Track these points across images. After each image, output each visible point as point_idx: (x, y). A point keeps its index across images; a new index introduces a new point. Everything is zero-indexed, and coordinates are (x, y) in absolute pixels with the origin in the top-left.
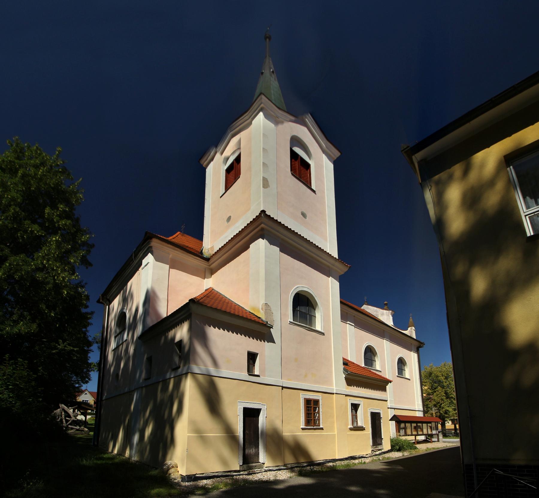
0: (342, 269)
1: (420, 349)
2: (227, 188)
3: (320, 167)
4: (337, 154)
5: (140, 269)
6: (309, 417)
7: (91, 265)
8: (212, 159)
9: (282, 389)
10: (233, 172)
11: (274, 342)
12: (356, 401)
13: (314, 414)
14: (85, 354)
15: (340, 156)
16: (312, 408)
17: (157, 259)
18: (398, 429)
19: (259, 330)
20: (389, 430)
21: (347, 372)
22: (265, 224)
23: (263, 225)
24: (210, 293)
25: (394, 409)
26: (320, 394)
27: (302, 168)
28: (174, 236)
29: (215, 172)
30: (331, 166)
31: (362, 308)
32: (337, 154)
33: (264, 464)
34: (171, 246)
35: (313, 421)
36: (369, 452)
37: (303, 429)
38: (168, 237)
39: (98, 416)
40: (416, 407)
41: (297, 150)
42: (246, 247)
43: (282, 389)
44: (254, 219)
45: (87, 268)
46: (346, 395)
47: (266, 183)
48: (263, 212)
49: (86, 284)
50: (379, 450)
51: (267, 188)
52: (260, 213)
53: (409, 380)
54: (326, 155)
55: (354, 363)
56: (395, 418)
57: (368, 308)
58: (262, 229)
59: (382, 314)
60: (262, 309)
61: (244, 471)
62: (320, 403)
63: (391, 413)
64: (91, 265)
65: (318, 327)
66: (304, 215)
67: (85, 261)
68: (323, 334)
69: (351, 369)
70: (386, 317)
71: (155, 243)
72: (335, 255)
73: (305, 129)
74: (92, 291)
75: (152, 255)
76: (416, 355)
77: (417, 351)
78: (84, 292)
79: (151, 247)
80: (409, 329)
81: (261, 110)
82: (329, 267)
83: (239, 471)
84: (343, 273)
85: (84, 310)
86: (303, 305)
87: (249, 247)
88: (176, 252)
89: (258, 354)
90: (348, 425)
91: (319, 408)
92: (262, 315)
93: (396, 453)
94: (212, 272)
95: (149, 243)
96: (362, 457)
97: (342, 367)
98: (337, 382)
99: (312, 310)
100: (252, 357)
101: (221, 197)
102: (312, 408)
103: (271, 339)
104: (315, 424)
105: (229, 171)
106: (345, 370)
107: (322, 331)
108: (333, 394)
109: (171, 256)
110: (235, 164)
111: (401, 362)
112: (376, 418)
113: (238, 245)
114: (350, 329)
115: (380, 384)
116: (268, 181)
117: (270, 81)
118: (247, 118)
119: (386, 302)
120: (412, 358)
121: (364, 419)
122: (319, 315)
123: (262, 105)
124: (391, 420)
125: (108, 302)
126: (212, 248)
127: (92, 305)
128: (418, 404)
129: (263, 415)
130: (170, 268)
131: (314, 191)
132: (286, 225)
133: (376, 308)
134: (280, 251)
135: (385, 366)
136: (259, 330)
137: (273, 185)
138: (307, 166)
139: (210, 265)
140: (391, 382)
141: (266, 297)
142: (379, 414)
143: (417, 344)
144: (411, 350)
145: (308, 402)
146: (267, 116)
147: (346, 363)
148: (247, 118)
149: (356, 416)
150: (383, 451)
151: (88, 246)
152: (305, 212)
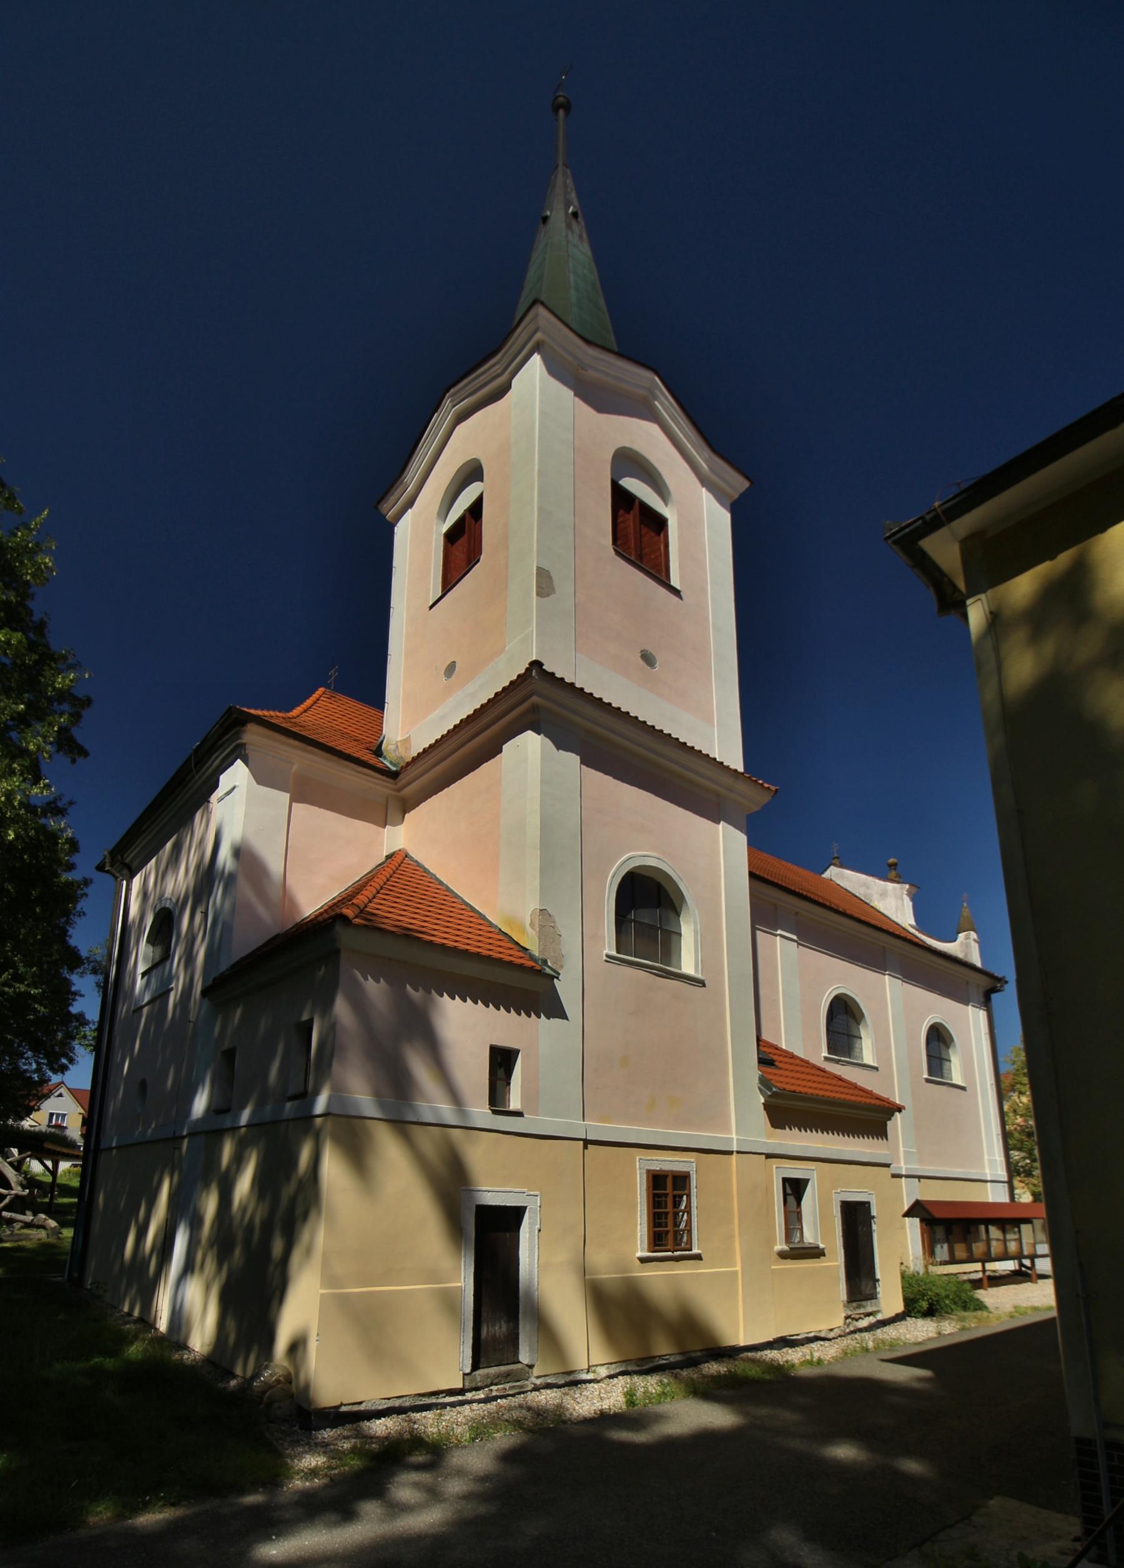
0: (755, 798)
1: (994, 996)
2: (448, 584)
3: (691, 523)
4: (739, 484)
5: (214, 798)
6: (660, 1225)
7: (84, 753)
8: (410, 503)
9: (585, 1147)
10: (463, 543)
11: (563, 1016)
12: (796, 1171)
13: (676, 1214)
14: (63, 994)
15: (748, 489)
16: (667, 1195)
17: (262, 777)
18: (929, 1249)
19: (525, 986)
20: (900, 1248)
21: (770, 1089)
22: (540, 695)
23: (535, 699)
24: (398, 861)
25: (920, 1177)
26: (692, 1157)
27: (645, 530)
28: (309, 702)
29: (416, 540)
30: (724, 518)
31: (826, 875)
32: (739, 484)
33: (531, 1367)
34: (296, 743)
35: (670, 1236)
36: (838, 1321)
37: (643, 1260)
38: (290, 710)
39: (89, 1174)
40: (987, 1171)
41: (633, 485)
42: (493, 750)
43: (585, 1147)
44: (512, 683)
45: (74, 761)
46: (769, 1156)
47: (545, 584)
48: (536, 664)
49: (71, 803)
50: (868, 1315)
51: (548, 595)
52: (527, 669)
53: (963, 1088)
54: (709, 490)
55: (793, 1056)
56: (917, 1209)
57: (842, 877)
58: (535, 708)
59: (883, 894)
60: (532, 925)
61: (477, 1389)
62: (693, 1183)
63: (908, 1193)
64: (84, 753)
65: (688, 966)
66: (648, 659)
67: (67, 744)
68: (702, 983)
69: (784, 1081)
70: (893, 902)
71: (252, 735)
72: (736, 762)
73: (654, 429)
74: (88, 831)
75: (246, 763)
76: (982, 1015)
77: (986, 1002)
78: (62, 830)
79: (242, 746)
80: (961, 936)
81: (538, 348)
82: (718, 795)
83: (461, 1392)
84: (756, 809)
85: (66, 877)
86: (647, 905)
87: (500, 751)
88: (310, 756)
89: (518, 1051)
90: (771, 1242)
91: (689, 1196)
92: (530, 941)
93: (920, 1322)
94: (406, 806)
95: (237, 735)
96: (817, 1339)
97: (754, 1072)
98: (740, 1117)
99: (672, 915)
100: (502, 1061)
101: (431, 607)
102: (667, 1195)
103: (556, 1011)
104: (677, 1246)
105: (451, 537)
106: (764, 1083)
107: (699, 976)
108: (730, 1153)
109: (295, 768)
110: (469, 521)
111: (939, 1039)
112: (856, 1219)
113: (474, 743)
114: (782, 950)
115: (870, 1117)
116: (550, 577)
117: (565, 250)
118: (497, 369)
119: (892, 860)
120: (970, 1025)
121: (821, 1225)
122: (688, 931)
123: (538, 336)
124: (907, 1214)
125: (125, 872)
126: (407, 741)
127: (84, 866)
128: (992, 1162)
129: (531, 1225)
130: (293, 800)
131: (676, 592)
132: (596, 695)
133: (863, 876)
134: (582, 762)
135: (885, 1054)
136: (525, 986)
137: (564, 587)
138: (659, 524)
139: (401, 787)
140: (900, 1109)
141: (544, 890)
142: (864, 1206)
143: (985, 982)
144: (966, 1002)
145: (657, 1180)
146: (555, 369)
147: (769, 1057)
148: (497, 369)
149: (799, 1214)
150: (880, 1317)
151: (80, 704)
152: (650, 649)
